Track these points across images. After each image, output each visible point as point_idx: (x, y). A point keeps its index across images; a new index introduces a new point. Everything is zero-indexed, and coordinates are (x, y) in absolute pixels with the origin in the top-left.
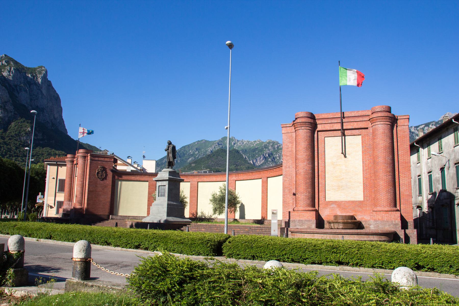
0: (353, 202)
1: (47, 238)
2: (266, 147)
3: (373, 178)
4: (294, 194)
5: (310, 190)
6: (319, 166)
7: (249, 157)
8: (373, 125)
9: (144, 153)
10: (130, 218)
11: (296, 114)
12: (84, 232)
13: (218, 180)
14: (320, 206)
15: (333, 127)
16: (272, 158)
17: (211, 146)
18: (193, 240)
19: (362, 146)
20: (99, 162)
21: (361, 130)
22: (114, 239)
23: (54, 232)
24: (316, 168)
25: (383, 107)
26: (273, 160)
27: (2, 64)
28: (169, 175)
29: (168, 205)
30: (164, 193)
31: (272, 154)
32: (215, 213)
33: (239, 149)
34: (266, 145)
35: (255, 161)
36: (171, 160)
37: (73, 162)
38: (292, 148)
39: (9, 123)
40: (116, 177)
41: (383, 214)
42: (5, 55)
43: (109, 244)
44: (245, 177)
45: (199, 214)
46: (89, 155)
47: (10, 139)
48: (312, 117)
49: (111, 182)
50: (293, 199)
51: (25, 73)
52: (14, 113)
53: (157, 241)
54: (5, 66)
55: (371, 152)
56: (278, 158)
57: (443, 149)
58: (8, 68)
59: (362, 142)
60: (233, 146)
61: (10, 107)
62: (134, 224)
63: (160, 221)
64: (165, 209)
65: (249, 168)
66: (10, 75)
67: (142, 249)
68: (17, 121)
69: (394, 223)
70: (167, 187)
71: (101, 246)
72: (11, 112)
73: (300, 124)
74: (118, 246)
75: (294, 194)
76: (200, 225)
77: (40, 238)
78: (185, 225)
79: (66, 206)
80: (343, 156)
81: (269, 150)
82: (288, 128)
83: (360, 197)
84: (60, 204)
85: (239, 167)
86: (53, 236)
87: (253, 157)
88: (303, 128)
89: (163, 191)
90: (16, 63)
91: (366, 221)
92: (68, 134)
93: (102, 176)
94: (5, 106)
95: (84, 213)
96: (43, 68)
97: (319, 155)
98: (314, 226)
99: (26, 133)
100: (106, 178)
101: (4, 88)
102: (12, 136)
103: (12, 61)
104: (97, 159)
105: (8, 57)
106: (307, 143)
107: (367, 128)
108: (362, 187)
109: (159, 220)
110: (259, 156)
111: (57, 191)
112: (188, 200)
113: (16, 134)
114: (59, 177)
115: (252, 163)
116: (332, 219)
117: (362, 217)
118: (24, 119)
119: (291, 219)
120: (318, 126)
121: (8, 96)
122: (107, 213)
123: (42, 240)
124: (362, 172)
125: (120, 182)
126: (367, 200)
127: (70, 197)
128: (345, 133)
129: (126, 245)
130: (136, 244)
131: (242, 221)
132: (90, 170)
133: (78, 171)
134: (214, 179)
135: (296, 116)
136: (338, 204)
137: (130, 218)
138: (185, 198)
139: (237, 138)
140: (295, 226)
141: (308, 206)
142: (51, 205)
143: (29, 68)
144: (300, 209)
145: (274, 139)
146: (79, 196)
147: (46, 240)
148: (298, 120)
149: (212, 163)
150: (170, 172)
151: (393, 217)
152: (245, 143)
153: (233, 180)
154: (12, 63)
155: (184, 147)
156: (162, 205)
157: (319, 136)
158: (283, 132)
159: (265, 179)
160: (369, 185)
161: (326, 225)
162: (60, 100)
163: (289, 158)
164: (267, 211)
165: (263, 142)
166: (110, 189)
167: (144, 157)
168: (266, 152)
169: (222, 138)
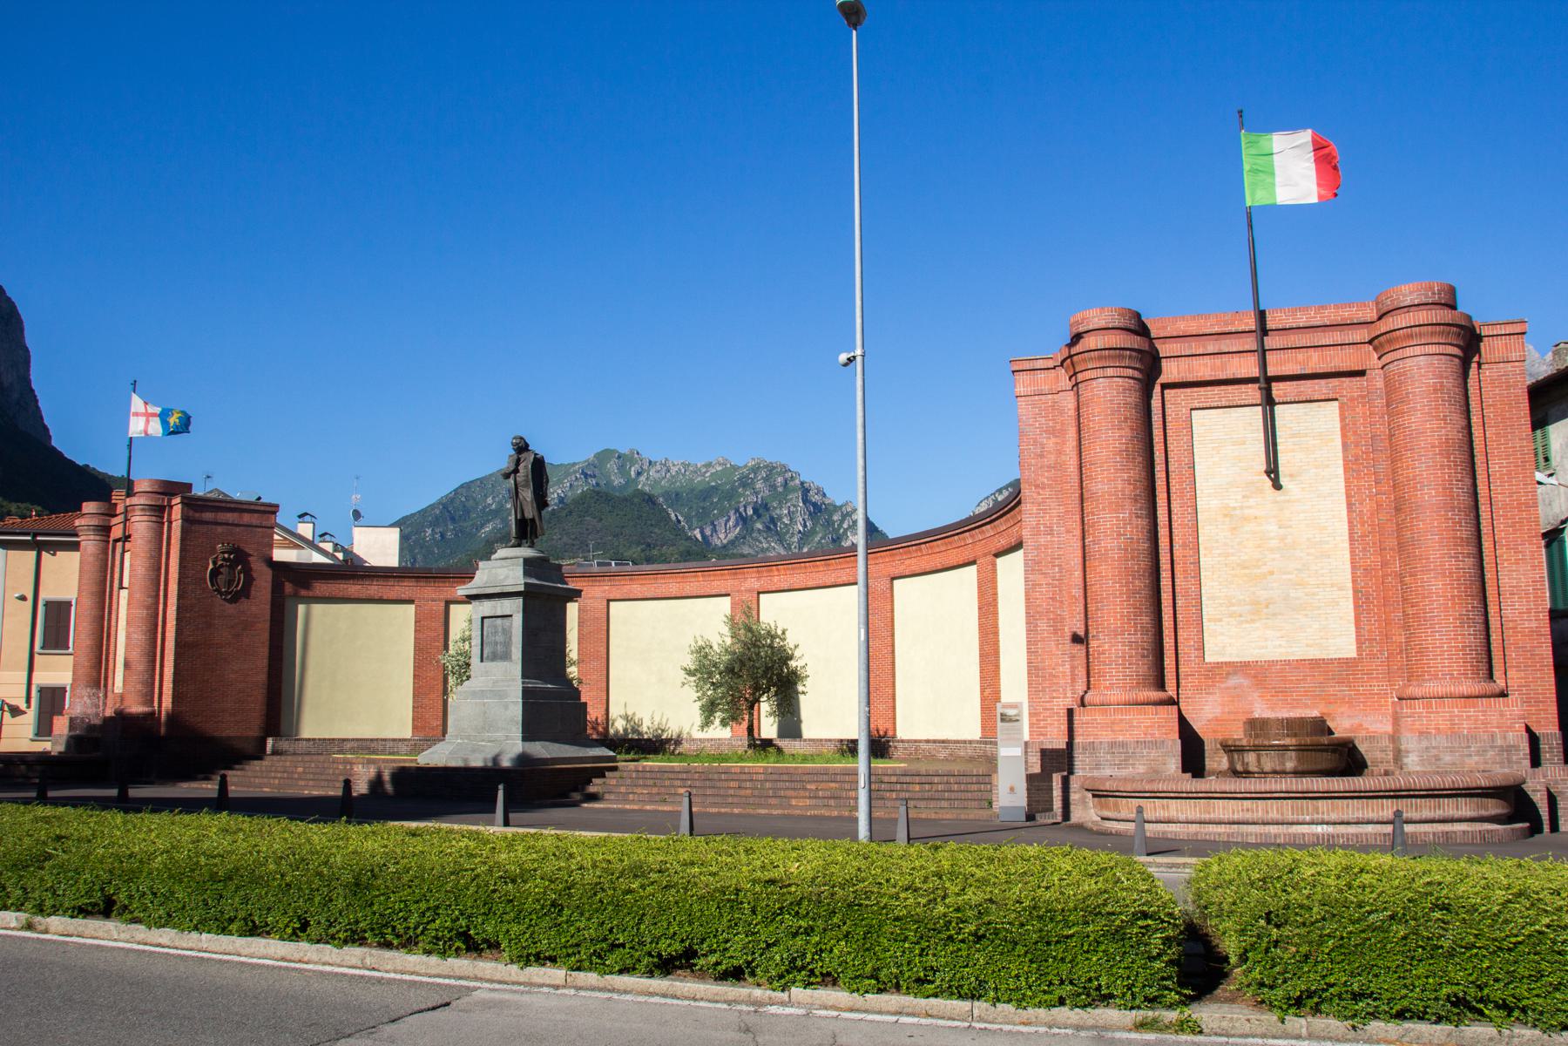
0: (1315, 664)
1: (83, 912)
2: (745, 482)
3: (1397, 566)
4: (1076, 639)
5: (1146, 619)
7: (688, 519)
8: (1385, 359)
9: (356, 499)
10: (348, 745)
11: (1079, 316)
12: (317, 882)
14: (1182, 682)
16: (766, 518)
17: (560, 482)
18: (1040, 913)
19: (1345, 445)
20: (220, 529)
21: (1335, 382)
22: (517, 919)
23: (131, 877)
24: (1163, 532)
25: (1431, 288)
26: (768, 528)
28: (526, 573)
29: (527, 693)
30: (507, 644)
31: (766, 507)
32: (707, 723)
33: (656, 492)
34: (747, 477)
35: (708, 532)
37: (105, 530)
38: (1060, 453)
40: (289, 588)
41: (1456, 709)
43: (473, 946)
45: (619, 726)
46: (178, 500)
48: (1140, 328)
50: (1073, 657)
53: (809, 931)
55: (1383, 466)
56: (786, 521)
57: (1554, 462)
59: (1343, 429)
60: (635, 481)
62: (387, 777)
63: (495, 759)
64: (516, 711)
65: (689, 553)
67: (701, 975)
69: (1499, 742)
70: (518, 620)
71: (434, 959)
73: (1100, 358)
74: (540, 959)
75: (1076, 639)
76: (662, 771)
77: (40, 909)
78: (601, 773)
79: (79, 705)
80: (1270, 483)
81: (757, 493)
82: (1041, 375)
83: (1344, 644)
84: (51, 700)
85: (655, 552)
86: (122, 897)
87: (704, 517)
88: (1110, 372)
89: (500, 638)
91: (1372, 738)
92: (54, 443)
93: (230, 583)
95: (163, 730)
97: (1173, 482)
98: (1173, 764)
100: (245, 593)
104: (208, 516)
106: (1127, 432)
107: (1361, 373)
108: (1347, 606)
109: (490, 756)
110: (723, 512)
111: (37, 648)
114: (47, 593)
115: (699, 537)
116: (1238, 734)
117: (1356, 721)
119: (1078, 740)
120: (1164, 363)
122: (254, 731)
123: (56, 922)
124: (1347, 545)
125: (301, 608)
126: (1372, 656)
127: (97, 671)
128: (1274, 393)
129: (601, 954)
130: (668, 948)
131: (786, 745)
132: (182, 559)
133: (132, 565)
135: (1078, 323)
136: (1257, 673)
137: (348, 745)
139: (648, 454)
140: (1098, 766)
141: (1142, 684)
144: (1113, 699)
146: (140, 666)
147: (80, 923)
148: (1091, 342)
149: (565, 539)
151: (1494, 719)
152: (674, 470)
153: (749, 591)
155: (467, 486)
156: (500, 695)
158: (1020, 390)
160: (1382, 592)
161: (1216, 760)
162: (20, 322)
163: (1047, 493)
165: (735, 468)
166: (266, 636)
167: (357, 515)
168: (747, 499)
169: (597, 456)
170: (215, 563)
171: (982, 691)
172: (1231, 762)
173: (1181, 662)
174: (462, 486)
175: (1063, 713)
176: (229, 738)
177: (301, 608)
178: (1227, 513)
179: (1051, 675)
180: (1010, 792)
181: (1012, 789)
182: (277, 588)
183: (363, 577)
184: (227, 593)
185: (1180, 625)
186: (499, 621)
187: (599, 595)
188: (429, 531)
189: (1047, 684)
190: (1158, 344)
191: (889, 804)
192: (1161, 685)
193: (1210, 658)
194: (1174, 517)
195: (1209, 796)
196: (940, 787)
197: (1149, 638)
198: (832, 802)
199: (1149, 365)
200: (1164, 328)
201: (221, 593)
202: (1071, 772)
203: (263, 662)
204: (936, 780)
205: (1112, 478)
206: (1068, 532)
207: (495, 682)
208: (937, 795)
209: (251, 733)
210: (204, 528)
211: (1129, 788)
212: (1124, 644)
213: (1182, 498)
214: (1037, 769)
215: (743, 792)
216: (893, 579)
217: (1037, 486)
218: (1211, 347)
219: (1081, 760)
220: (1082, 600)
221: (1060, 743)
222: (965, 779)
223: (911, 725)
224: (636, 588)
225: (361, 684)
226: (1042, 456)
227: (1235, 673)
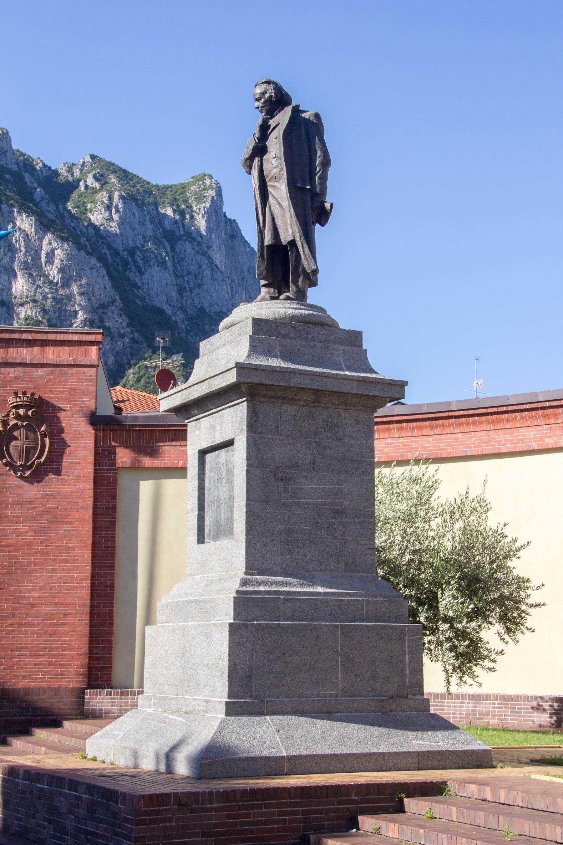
20: (13, 372)
27: (86, 187)
36: (289, 230)
40: (124, 457)
42: (93, 157)
51: (156, 205)
52: (133, 339)
54: (95, 191)
61: (117, 320)
66: (111, 219)
72: (122, 336)
90: (125, 176)
93: (29, 452)
94: (102, 320)
96: (208, 182)
100: (52, 465)
101: (94, 261)
103: (114, 172)
105: (100, 160)
121: (109, 285)
125: (146, 487)
143: (166, 188)
154: (113, 179)
166: (87, 531)
176: (28, 691)
177: (146, 487)
182: (103, 458)
184: (25, 467)
203: (82, 571)
209: (64, 683)
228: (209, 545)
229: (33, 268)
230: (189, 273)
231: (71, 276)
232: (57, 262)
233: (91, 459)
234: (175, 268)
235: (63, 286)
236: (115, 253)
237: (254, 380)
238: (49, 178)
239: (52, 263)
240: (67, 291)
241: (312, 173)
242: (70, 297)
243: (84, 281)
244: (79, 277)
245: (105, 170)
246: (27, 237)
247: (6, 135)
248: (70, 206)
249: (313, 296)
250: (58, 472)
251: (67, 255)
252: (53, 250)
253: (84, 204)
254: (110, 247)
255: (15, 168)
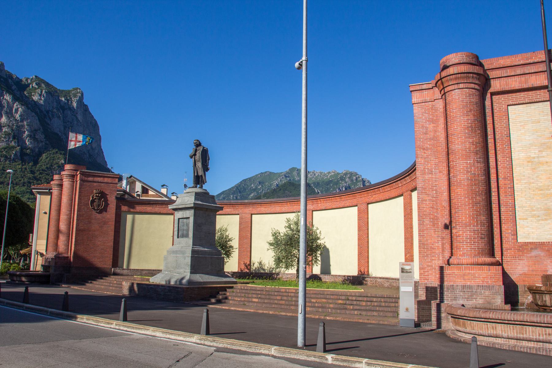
2: (342, 179)
5: (483, 218)
6: (499, 167)
10: (144, 272)
13: (284, 210)
14: (505, 253)
15: (526, 81)
17: (277, 179)
20: (95, 184)
24: (493, 171)
27: (32, 87)
28: (196, 199)
29: (193, 252)
30: (188, 230)
31: (349, 187)
36: (201, 173)
39: (40, 154)
42: (36, 77)
44: (328, 204)
45: (255, 266)
47: (41, 173)
49: (114, 216)
50: (443, 238)
51: (58, 96)
52: (46, 143)
54: (36, 89)
58: (39, 91)
61: (40, 136)
64: (188, 260)
66: (41, 99)
68: (48, 152)
70: (191, 220)
72: (42, 142)
73: (456, 79)
81: (346, 183)
82: (425, 92)
88: (461, 86)
89: (185, 228)
90: (48, 85)
93: (99, 205)
94: (34, 135)
96: (79, 91)
98: (499, 300)
99: (59, 167)
100: (105, 209)
101: (33, 114)
102: (43, 170)
103: (44, 83)
104: (91, 179)
106: (471, 117)
112: (235, 243)
113: (47, 168)
118: (57, 150)
119: (446, 284)
120: (492, 82)
121: (38, 123)
125: (129, 217)
131: (325, 278)
132: (79, 196)
134: (278, 208)
137: (144, 272)
138: (230, 240)
140: (455, 299)
141: (481, 253)
142: (41, 252)
143: (63, 91)
144: (464, 261)
145: (351, 170)
148: (451, 70)
150: (197, 194)
152: (317, 175)
154: (43, 85)
155: (245, 181)
156: (183, 253)
157: (494, 104)
159: (363, 207)
161: (526, 298)
164: (368, 262)
165: (338, 174)
169: (290, 170)
170: (93, 197)
171: (406, 255)
172: (535, 298)
173: (504, 241)
174: (243, 180)
175: (437, 268)
177: (129, 217)
178: (530, 161)
179: (431, 247)
180: (407, 310)
181: (407, 309)
182: (118, 208)
183: (153, 204)
185: (503, 221)
186: (185, 220)
187: (248, 212)
188: (232, 196)
189: (429, 252)
190: (488, 72)
191: (348, 312)
192: (492, 255)
193: (520, 240)
194: (499, 163)
195: (523, 324)
196: (376, 304)
197: (485, 228)
198: (320, 310)
199: (483, 83)
200: (492, 64)
201: (95, 210)
202: (442, 300)
204: (374, 299)
205: (463, 142)
206: (440, 172)
207: (182, 247)
208: (373, 308)
210: (88, 184)
211: (471, 315)
212: (470, 231)
213: (503, 153)
214: (423, 297)
215: (281, 302)
216: (368, 204)
217: (424, 149)
218: (519, 71)
219: (447, 294)
220: (448, 208)
221: (434, 282)
222: (389, 300)
223: (377, 270)
224: (263, 209)
225: (158, 248)
226: (426, 134)
227: (536, 248)
228: (180, 239)
229: (10, 114)
230: (68, 122)
231: (24, 118)
232: (19, 113)
233: (115, 208)
234: (64, 120)
235: (21, 122)
236: (41, 111)
237: (196, 206)
238: (18, 82)
239: (17, 113)
240: (22, 123)
241: (206, 161)
242: (23, 126)
243: (29, 121)
244: (27, 119)
245: (40, 82)
246: (8, 102)
247: (2, 64)
248: (25, 93)
249: (205, 187)
250: (106, 211)
251: (23, 110)
252: (18, 108)
253: (31, 93)
254: (39, 109)
255: (5, 77)
